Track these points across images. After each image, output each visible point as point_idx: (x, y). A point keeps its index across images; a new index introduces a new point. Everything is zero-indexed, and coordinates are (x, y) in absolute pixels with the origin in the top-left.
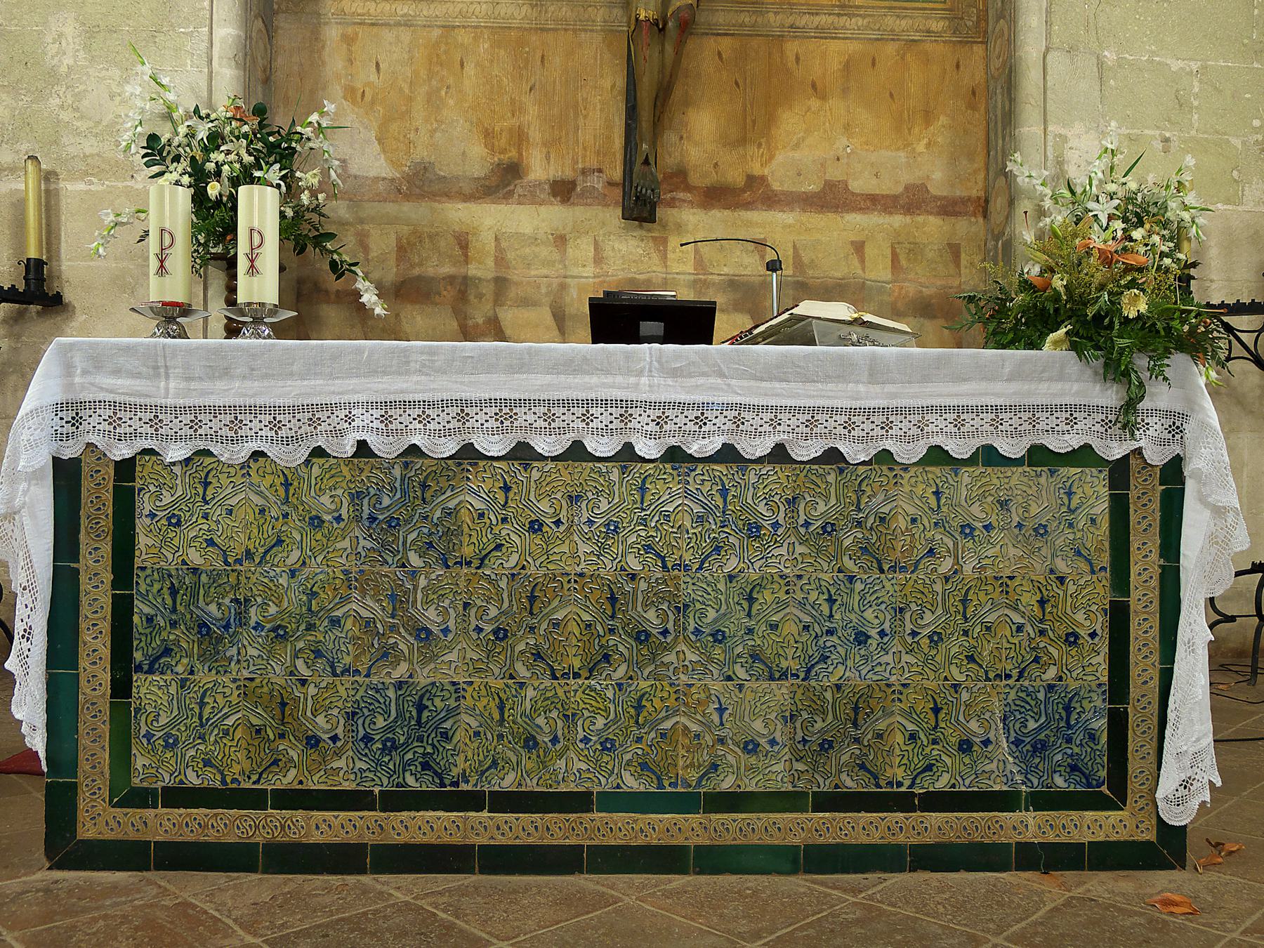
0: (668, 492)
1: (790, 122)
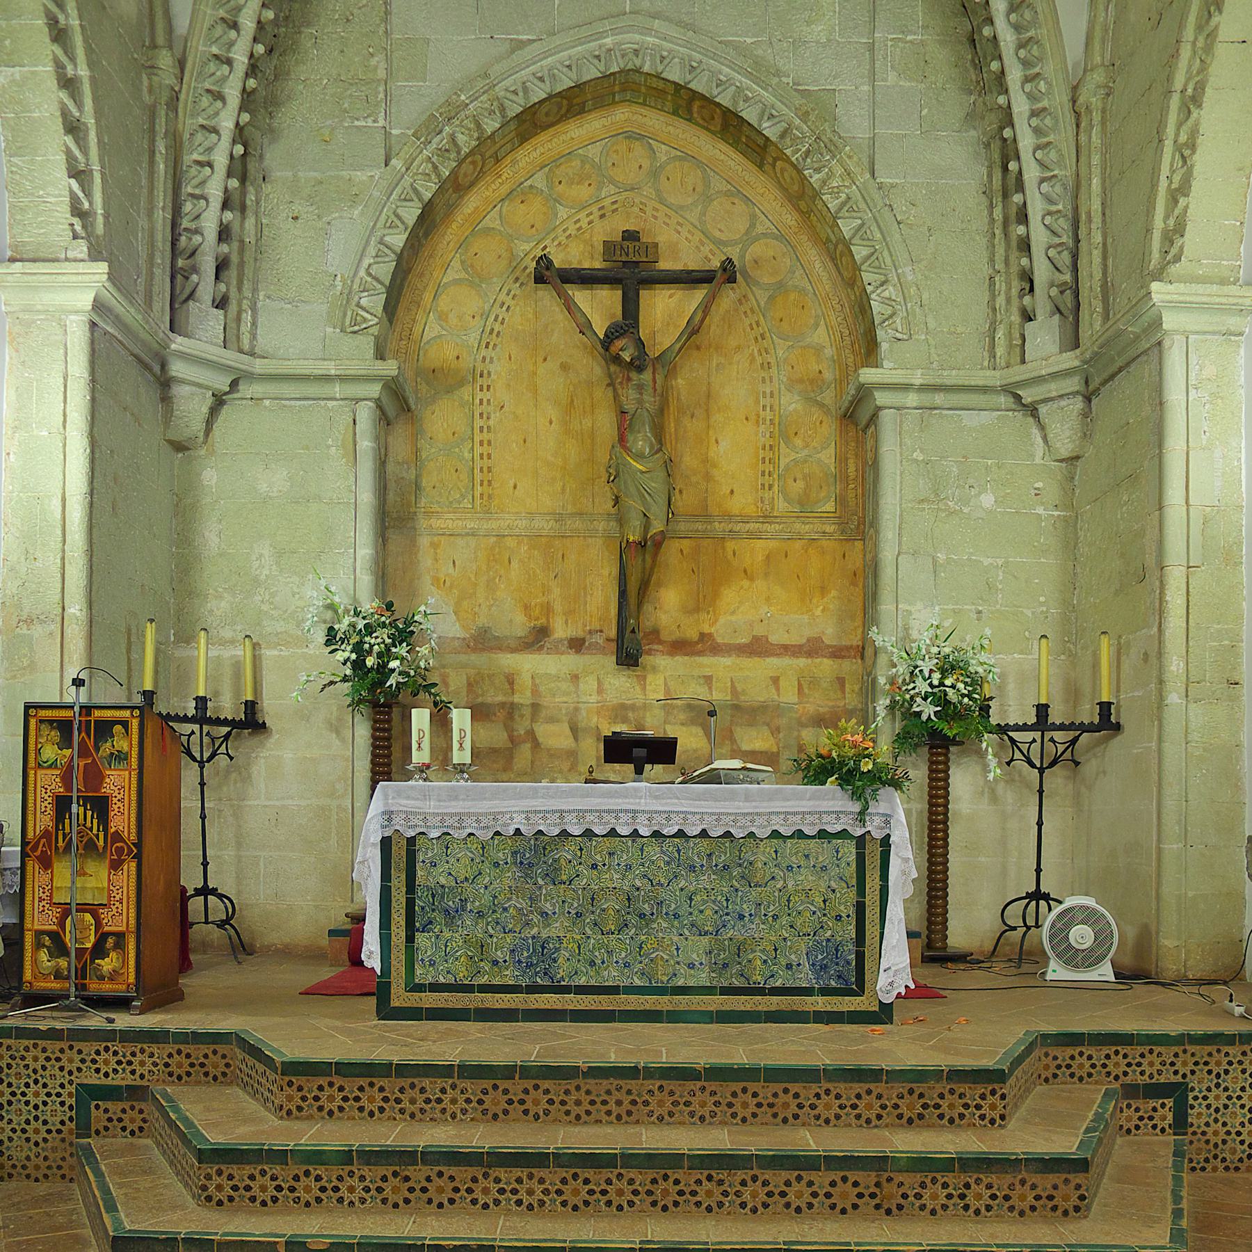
0: (653, 850)
1: (729, 596)
